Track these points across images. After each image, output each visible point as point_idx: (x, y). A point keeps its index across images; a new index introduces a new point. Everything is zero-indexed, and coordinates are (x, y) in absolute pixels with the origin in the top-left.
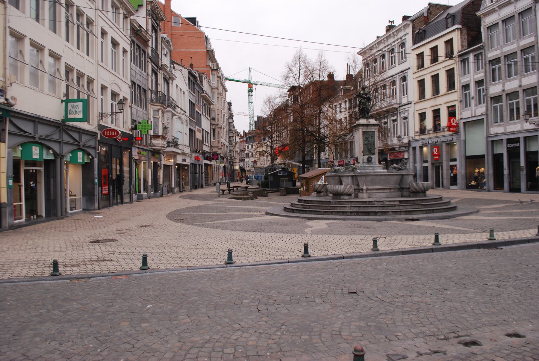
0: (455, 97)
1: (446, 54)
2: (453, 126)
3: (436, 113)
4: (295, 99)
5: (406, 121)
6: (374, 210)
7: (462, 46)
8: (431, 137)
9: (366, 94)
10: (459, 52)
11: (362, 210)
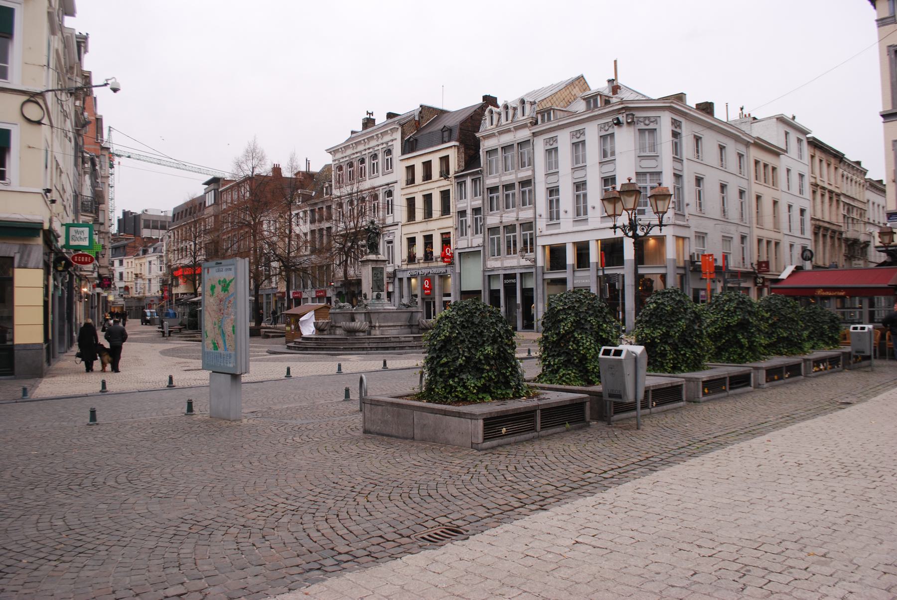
0: (449, 223)
1: (441, 172)
2: (448, 257)
3: (428, 240)
4: (218, 196)
5: (390, 245)
6: (392, 345)
7: (459, 166)
8: (420, 266)
9: (375, 229)
10: (456, 173)
11: (380, 345)
